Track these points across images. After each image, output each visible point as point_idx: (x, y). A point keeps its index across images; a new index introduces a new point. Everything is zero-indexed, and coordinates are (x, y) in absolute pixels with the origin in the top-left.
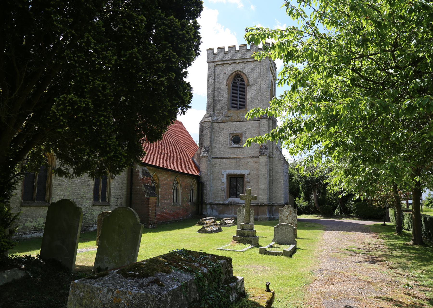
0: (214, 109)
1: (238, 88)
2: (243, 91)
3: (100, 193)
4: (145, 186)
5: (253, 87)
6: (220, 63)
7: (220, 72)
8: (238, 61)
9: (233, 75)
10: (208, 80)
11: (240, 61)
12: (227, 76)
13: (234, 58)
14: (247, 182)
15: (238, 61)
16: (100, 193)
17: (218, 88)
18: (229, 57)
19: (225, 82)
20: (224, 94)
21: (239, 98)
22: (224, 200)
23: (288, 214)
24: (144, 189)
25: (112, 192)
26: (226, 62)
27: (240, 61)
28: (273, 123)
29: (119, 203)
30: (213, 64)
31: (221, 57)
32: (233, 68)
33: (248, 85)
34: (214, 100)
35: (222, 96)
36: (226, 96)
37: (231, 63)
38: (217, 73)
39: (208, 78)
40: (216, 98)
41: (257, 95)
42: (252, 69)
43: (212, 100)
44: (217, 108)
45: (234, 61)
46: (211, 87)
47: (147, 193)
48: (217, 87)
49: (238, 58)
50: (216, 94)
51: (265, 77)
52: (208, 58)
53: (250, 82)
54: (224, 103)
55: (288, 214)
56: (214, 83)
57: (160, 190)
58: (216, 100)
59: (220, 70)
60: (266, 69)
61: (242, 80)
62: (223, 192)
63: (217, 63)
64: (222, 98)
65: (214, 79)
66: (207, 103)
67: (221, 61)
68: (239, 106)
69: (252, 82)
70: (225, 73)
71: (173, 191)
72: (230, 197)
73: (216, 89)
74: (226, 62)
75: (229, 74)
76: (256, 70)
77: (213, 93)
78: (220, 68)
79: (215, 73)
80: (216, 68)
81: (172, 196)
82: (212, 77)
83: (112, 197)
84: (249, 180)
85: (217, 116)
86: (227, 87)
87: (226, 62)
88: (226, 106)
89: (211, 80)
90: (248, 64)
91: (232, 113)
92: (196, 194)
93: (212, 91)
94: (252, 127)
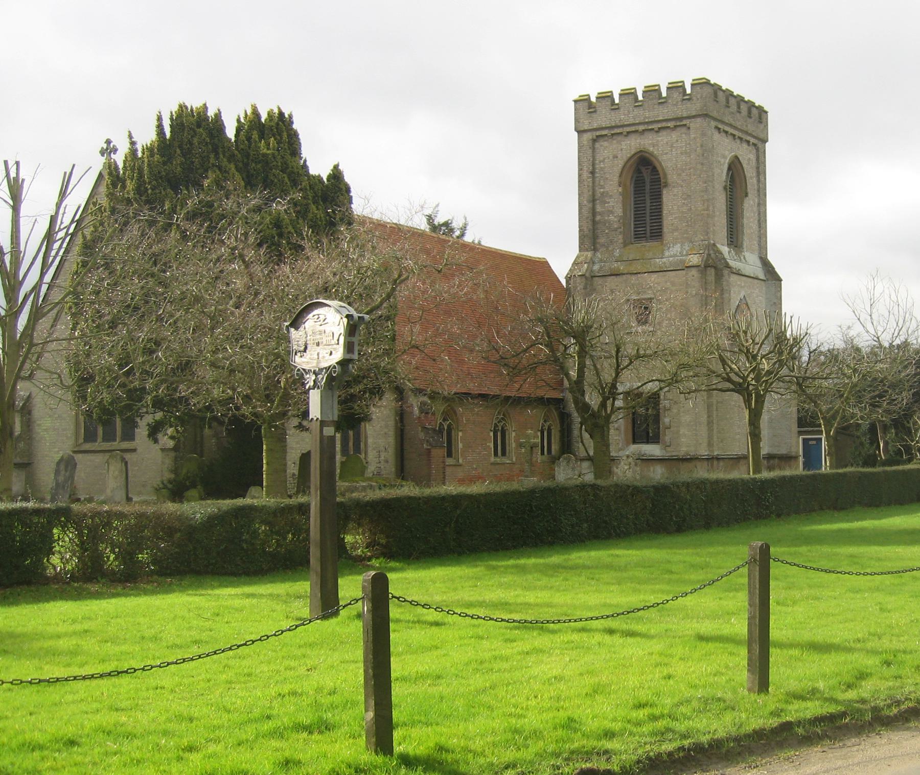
0: (594, 244)
1: (647, 190)
2: (657, 197)
3: (351, 444)
4: (424, 428)
5: (676, 190)
6: (604, 132)
7: (606, 153)
8: (641, 128)
9: (632, 160)
10: (580, 175)
11: (645, 127)
12: (621, 163)
13: (631, 121)
14: (666, 410)
15: (641, 128)
16: (351, 444)
17: (602, 194)
18: (622, 117)
19: (616, 179)
20: (615, 207)
21: (648, 214)
22: (620, 450)
23: (626, 467)
24: (422, 435)
25: (370, 441)
26: (615, 132)
27: (645, 127)
28: (716, 274)
29: (383, 458)
30: (588, 136)
31: (604, 118)
32: (629, 146)
33: (666, 186)
34: (594, 222)
35: (612, 212)
36: (619, 211)
37: (628, 133)
38: (599, 157)
39: (580, 170)
40: (598, 218)
41: (685, 209)
42: (672, 146)
43: (591, 223)
44: (602, 240)
45: (633, 129)
46: (586, 191)
47: (427, 441)
48: (599, 191)
49: (641, 119)
50: (599, 208)
51: (699, 166)
52: (577, 120)
53: (669, 177)
54: (616, 230)
55: (626, 467)
56: (594, 183)
57: (460, 434)
58: (599, 222)
59: (606, 150)
60: (702, 146)
61: (655, 170)
62: (617, 432)
63: (598, 133)
64: (612, 217)
65: (593, 173)
66: (580, 231)
67: (606, 128)
68: (648, 234)
69: (672, 177)
70: (615, 157)
71: (492, 434)
72: (634, 442)
73: (598, 195)
74: (615, 132)
75: (625, 159)
76: (681, 147)
77: (590, 205)
78: (605, 144)
79: (594, 157)
80: (597, 145)
81: (492, 445)
82: (587, 167)
83: (370, 449)
84: (668, 406)
85: (601, 261)
86: (620, 189)
87: (618, 131)
88: (621, 237)
89: (586, 175)
90: (664, 133)
91: (633, 251)
92: (558, 438)
93: (589, 201)
94: (673, 284)
